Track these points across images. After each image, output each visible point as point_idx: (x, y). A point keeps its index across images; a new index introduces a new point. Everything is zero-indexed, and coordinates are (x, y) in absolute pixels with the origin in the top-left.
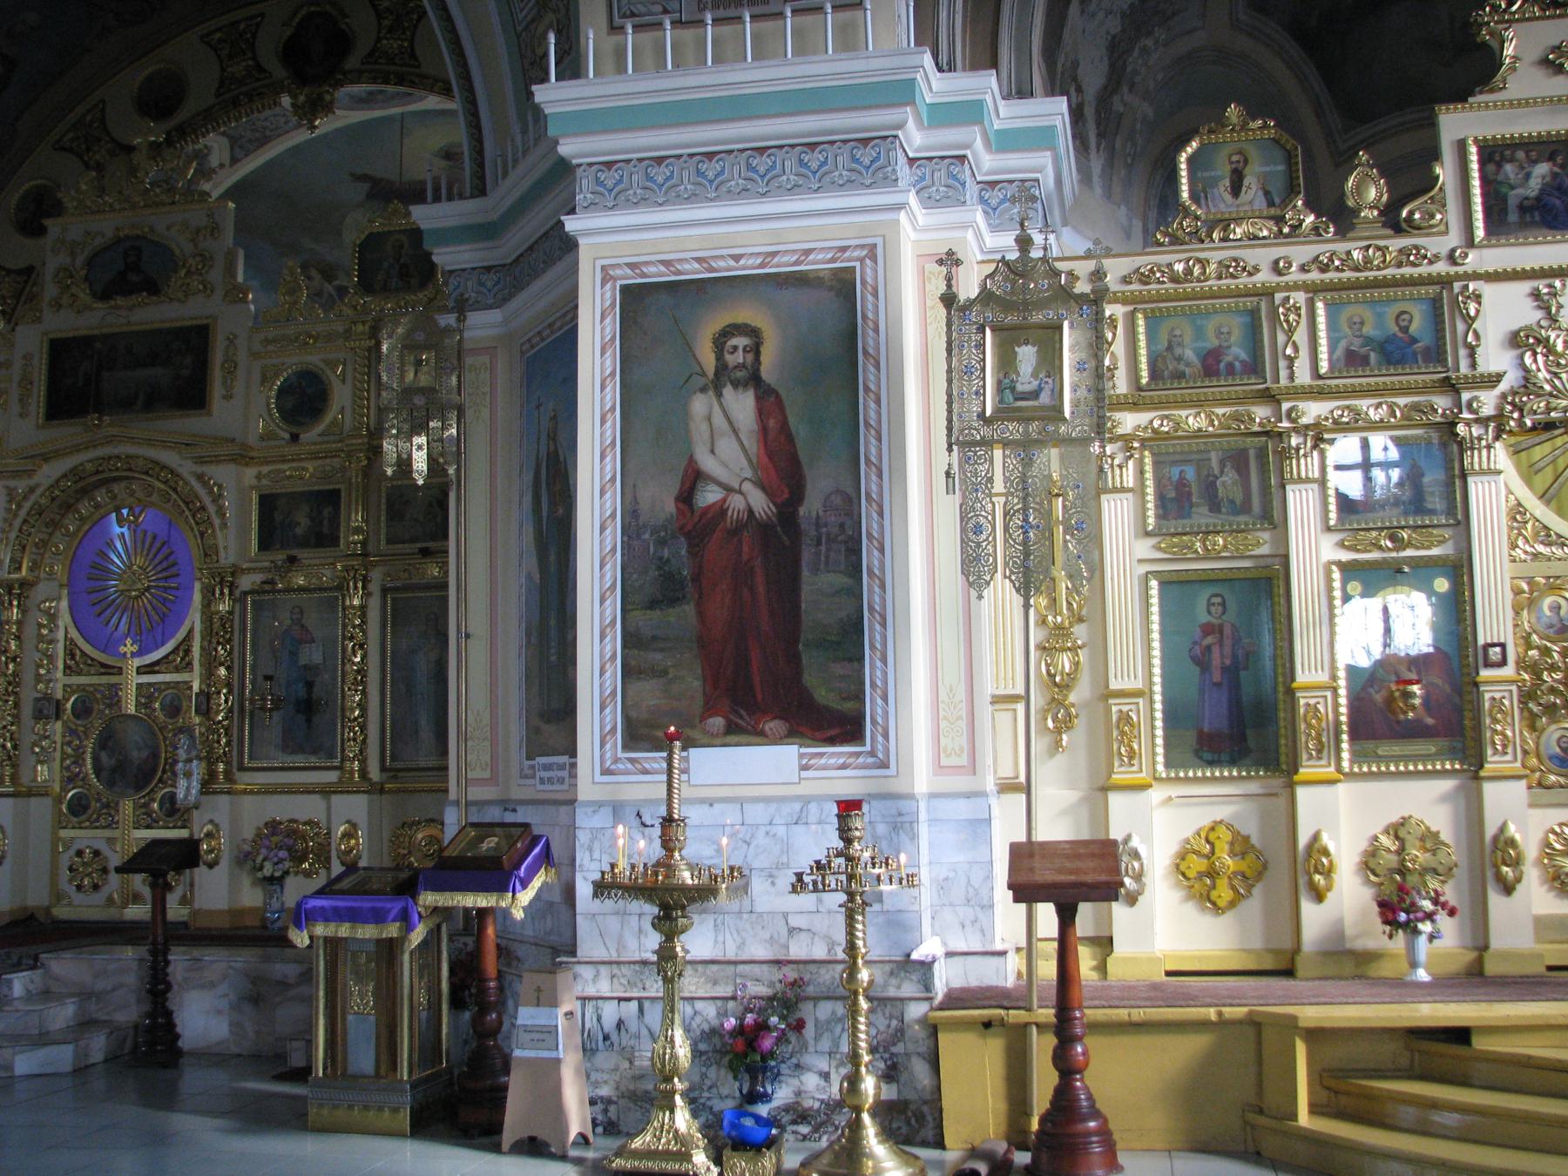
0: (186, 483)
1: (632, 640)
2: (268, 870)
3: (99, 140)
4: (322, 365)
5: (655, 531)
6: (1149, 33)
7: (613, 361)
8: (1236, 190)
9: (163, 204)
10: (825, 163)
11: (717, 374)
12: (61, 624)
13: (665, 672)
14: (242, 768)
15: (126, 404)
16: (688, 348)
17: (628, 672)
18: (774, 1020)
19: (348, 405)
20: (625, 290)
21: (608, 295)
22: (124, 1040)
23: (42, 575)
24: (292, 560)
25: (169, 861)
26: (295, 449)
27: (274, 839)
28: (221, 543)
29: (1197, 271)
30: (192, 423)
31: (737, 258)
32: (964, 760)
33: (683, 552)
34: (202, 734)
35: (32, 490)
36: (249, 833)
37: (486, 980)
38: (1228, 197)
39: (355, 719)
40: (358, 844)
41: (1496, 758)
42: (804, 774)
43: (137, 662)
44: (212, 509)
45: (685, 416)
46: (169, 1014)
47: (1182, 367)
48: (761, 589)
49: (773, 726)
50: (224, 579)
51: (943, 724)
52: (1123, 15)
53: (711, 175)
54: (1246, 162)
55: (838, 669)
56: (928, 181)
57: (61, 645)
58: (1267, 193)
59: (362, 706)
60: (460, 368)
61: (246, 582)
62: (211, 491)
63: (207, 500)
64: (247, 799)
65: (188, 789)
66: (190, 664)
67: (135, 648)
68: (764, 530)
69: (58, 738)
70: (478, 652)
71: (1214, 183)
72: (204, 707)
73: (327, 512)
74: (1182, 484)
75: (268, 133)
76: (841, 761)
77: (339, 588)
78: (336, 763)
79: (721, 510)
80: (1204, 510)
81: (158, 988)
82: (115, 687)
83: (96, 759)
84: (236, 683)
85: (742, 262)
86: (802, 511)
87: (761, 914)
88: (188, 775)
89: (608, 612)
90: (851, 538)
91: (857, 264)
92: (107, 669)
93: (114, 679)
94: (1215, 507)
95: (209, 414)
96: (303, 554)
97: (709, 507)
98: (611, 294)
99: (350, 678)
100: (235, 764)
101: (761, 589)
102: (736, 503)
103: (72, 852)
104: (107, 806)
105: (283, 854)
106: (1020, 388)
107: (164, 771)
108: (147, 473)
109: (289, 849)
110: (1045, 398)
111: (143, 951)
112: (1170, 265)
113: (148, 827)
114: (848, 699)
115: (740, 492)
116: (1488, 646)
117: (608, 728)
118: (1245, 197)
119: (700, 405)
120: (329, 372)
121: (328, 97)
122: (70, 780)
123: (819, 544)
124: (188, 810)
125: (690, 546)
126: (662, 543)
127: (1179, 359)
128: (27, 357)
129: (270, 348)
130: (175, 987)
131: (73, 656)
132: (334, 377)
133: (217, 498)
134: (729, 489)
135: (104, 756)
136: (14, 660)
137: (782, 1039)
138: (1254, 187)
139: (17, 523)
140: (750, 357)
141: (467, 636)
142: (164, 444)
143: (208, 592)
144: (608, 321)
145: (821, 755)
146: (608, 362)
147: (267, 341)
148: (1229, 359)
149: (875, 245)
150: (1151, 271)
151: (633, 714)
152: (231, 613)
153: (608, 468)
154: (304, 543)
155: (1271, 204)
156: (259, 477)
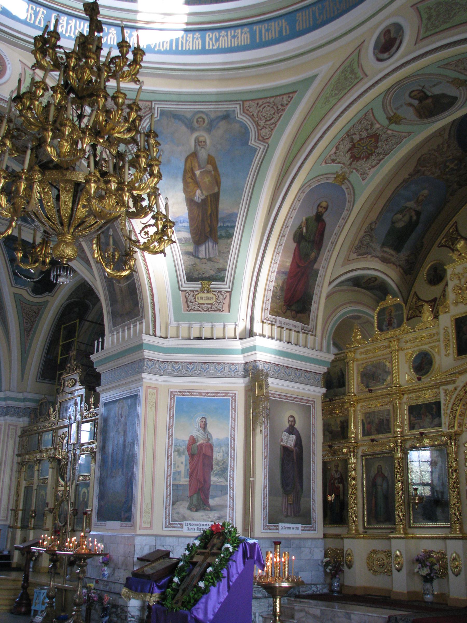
10: (193, 368)
14: (410, 527)
23: (464, 429)
35: (455, 389)
128: (445, 329)
136: (455, 471)
139: (450, 406)
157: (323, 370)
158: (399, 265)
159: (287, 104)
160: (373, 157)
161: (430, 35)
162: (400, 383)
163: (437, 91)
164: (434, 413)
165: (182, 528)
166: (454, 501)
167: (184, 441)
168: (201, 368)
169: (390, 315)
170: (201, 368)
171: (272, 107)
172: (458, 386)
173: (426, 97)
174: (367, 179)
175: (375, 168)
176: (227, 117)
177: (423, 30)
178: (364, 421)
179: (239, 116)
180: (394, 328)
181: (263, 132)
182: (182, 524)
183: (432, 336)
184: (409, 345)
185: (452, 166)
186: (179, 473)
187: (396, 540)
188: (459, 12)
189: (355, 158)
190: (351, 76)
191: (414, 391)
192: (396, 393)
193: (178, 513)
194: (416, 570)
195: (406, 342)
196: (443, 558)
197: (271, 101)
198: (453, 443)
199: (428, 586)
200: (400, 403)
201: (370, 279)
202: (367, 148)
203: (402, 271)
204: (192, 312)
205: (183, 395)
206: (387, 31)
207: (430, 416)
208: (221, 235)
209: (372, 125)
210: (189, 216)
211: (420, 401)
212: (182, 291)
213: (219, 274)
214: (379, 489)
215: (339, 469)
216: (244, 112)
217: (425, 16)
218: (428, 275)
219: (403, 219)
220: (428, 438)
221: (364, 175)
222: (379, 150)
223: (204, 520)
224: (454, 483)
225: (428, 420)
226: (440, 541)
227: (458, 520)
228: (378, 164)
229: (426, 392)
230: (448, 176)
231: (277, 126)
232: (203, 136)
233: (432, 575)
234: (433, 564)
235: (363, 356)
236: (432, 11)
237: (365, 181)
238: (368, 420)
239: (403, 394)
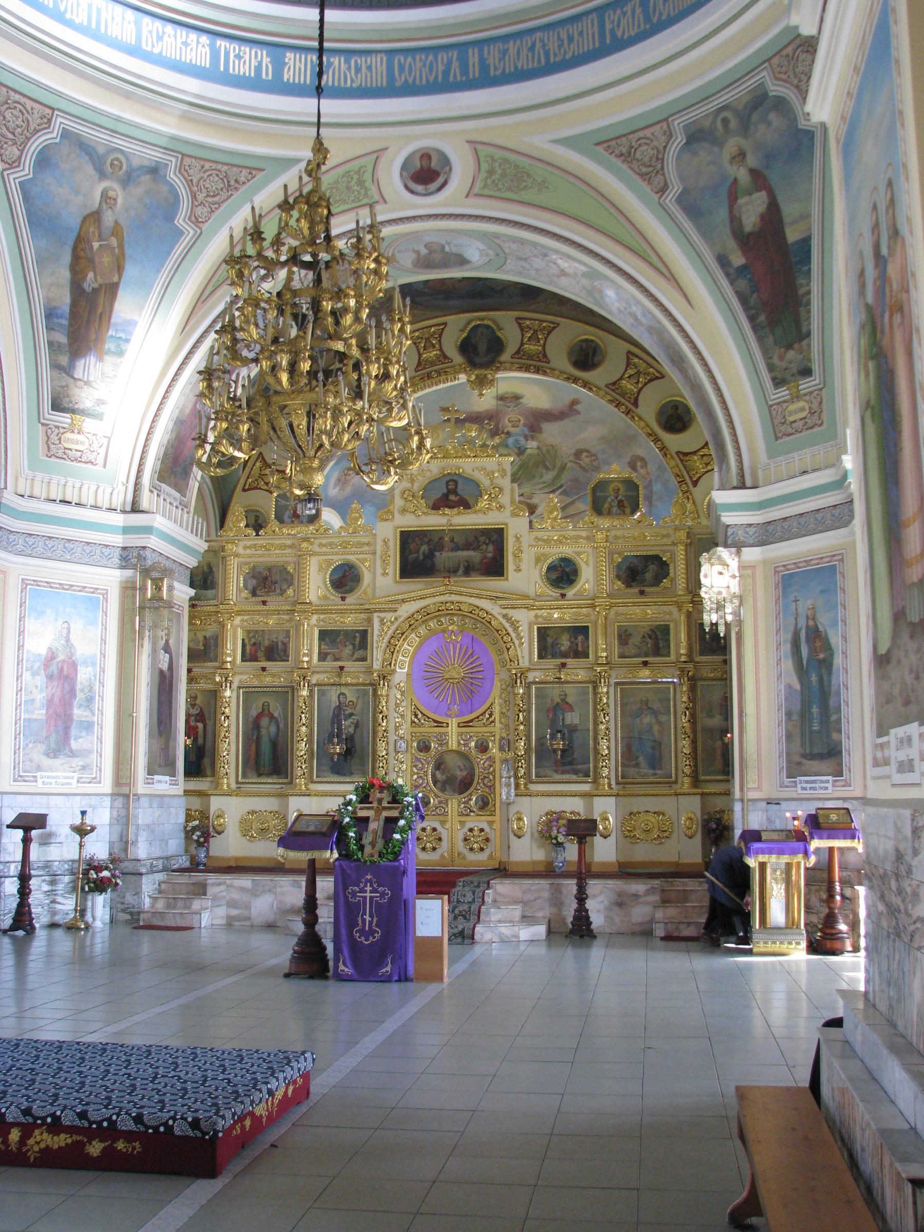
9: (469, 457)
14: (313, 782)
15: (452, 571)
19: (591, 578)
24: (564, 665)
30: (494, 584)
44: (513, 635)
63: (510, 630)
82: (446, 734)
83: (433, 776)
92: (439, 724)
95: (507, 579)
96: (570, 661)
103: (466, 830)
121: (489, 376)
131: (416, 716)
133: (516, 629)
154: (565, 655)
157: (192, 562)
159: (244, 183)
161: (491, 197)
164: (357, 643)
165: (36, 781)
167: (39, 655)
168: (65, 547)
170: (65, 547)
171: (222, 179)
172: (400, 617)
176: (155, 171)
177: (479, 184)
178: (246, 641)
179: (172, 176)
180: (302, 522)
181: (199, 211)
182: (795, 782)
186: (33, 701)
187: (217, 797)
188: (531, 188)
193: (31, 761)
197: (223, 170)
204: (53, 459)
205: (38, 586)
207: (351, 647)
208: (109, 349)
210: (71, 310)
212: (43, 424)
213: (97, 408)
214: (264, 732)
215: (198, 702)
216: (180, 172)
217: (485, 167)
223: (65, 771)
225: (348, 650)
231: (222, 208)
232: (114, 190)
235: (248, 551)
238: (253, 640)
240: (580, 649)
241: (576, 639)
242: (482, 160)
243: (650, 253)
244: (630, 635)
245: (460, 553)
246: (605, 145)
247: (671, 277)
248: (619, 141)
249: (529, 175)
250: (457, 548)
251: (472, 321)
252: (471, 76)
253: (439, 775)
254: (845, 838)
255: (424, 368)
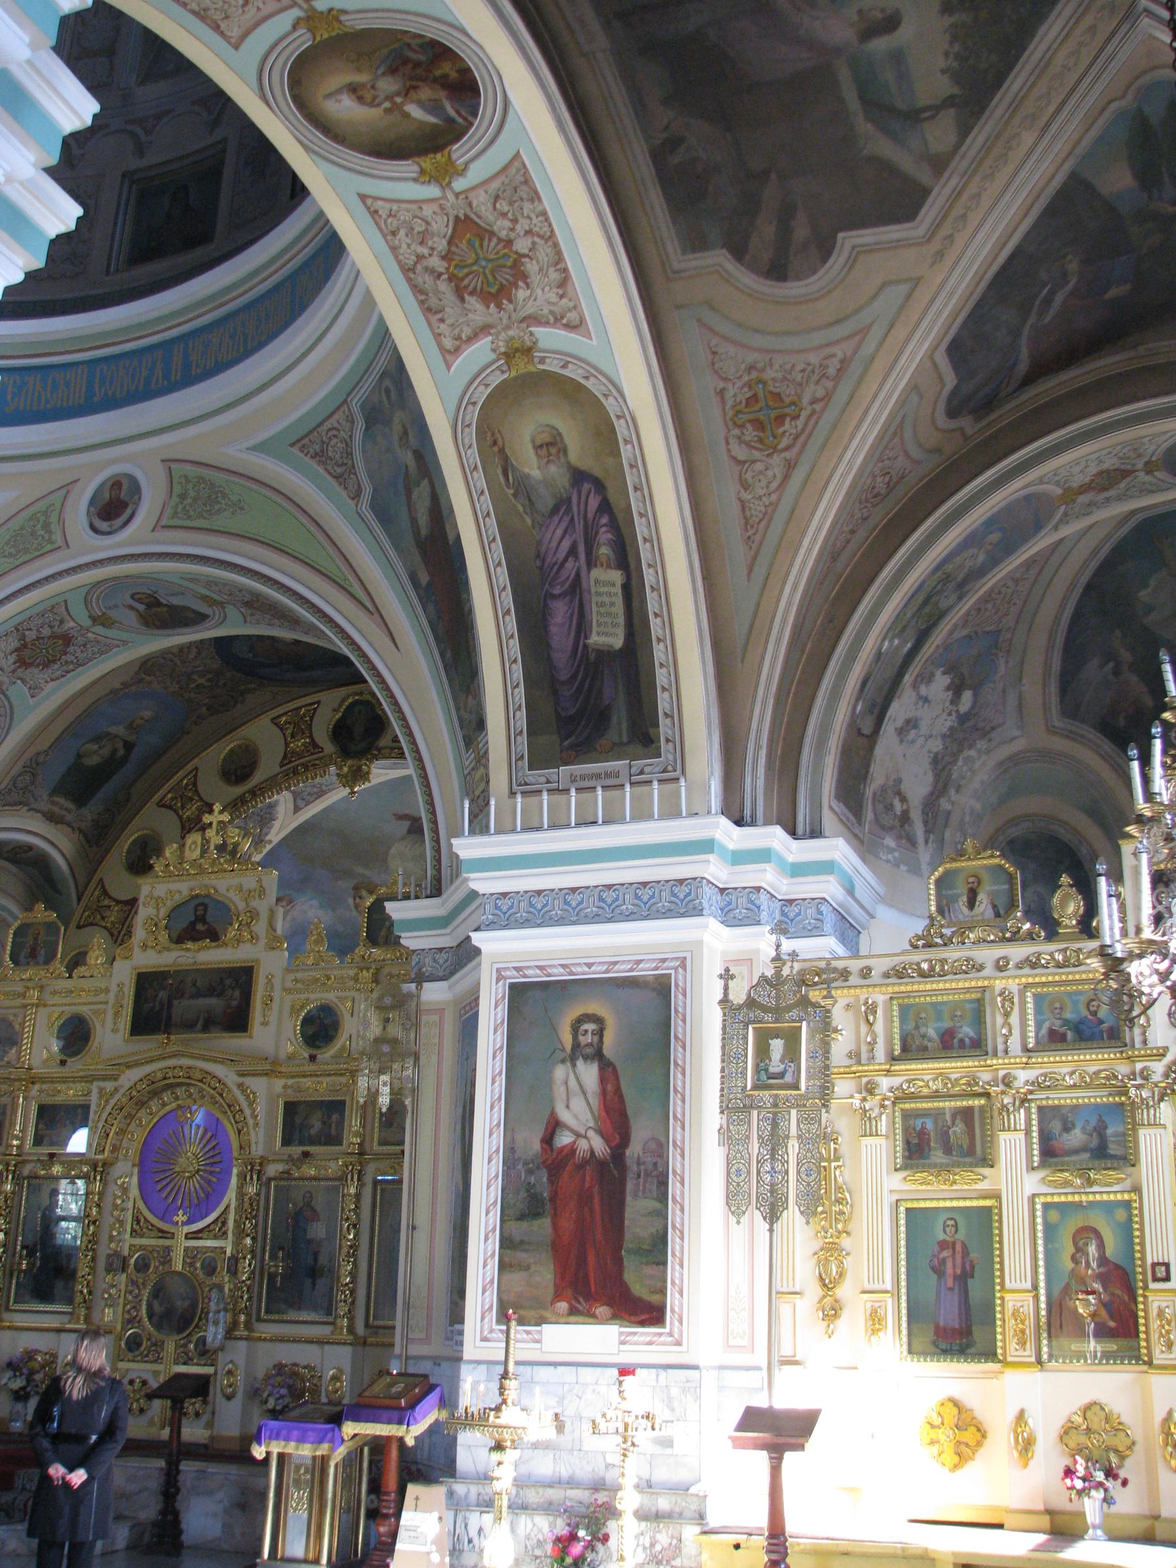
0: (230, 1091)
1: (507, 1243)
2: (271, 1404)
3: (191, 799)
4: (337, 1001)
5: (526, 1164)
6: (970, 747)
7: (501, 1038)
8: (971, 904)
11: (573, 1049)
12: (131, 1196)
13: (527, 1268)
14: (259, 1320)
16: (554, 1029)
17: (502, 1266)
18: (581, 1533)
20: (513, 986)
21: (500, 990)
22: (143, 1533)
25: (186, 1392)
26: (313, 1067)
27: (279, 1379)
28: (253, 1139)
29: (937, 969)
30: (234, 1042)
31: (589, 965)
32: (745, 1342)
33: (545, 1180)
34: (230, 1290)
35: (116, 1090)
36: (260, 1374)
37: (567, 1554)
38: (965, 910)
39: (347, 1284)
40: (342, 1386)
41: (1163, 1356)
42: (623, 1347)
43: (186, 1229)
44: (248, 1112)
45: (550, 1083)
46: (176, 1514)
47: (926, 1042)
48: (597, 1208)
49: (602, 1310)
50: (255, 1168)
51: (732, 1313)
52: (944, 736)
53: (574, 904)
54: (979, 883)
55: (649, 1270)
56: (733, 905)
57: (130, 1212)
58: (994, 907)
59: (353, 1275)
60: (417, 1025)
61: (272, 1170)
62: (248, 1096)
64: (262, 1345)
65: (215, 1334)
66: (225, 1233)
67: (185, 1218)
68: (601, 1166)
69: (123, 1287)
70: (422, 1237)
71: (955, 899)
72: (233, 1268)
73: (335, 1117)
74: (922, 1133)
75: (324, 788)
76: (648, 1339)
77: (339, 1179)
78: (331, 1319)
79: (572, 1149)
80: (940, 1153)
81: (170, 1490)
82: (168, 1249)
84: (259, 1251)
85: (593, 968)
86: (628, 1152)
87: (587, 1452)
88: (216, 1323)
89: (491, 1221)
90: (662, 1173)
91: (672, 972)
92: (163, 1234)
93: (167, 1242)
94: (948, 1150)
97: (566, 1146)
98: (502, 990)
99: (345, 1250)
100: (254, 1317)
101: (597, 1208)
102: (583, 1145)
104: (155, 1344)
105: (283, 1391)
106: (771, 1070)
107: (200, 1319)
108: (201, 1081)
109: (290, 1387)
110: (788, 1078)
111: (162, 1463)
112: (918, 964)
113: (185, 1364)
114: (655, 1292)
115: (585, 1137)
116: (1154, 1265)
117: (487, 1307)
118: (978, 909)
119: (560, 1072)
120: (342, 1007)
122: (130, 1322)
123: (639, 1176)
124: (215, 1352)
125: (550, 1175)
126: (530, 1172)
127: (923, 1036)
128: (120, 986)
129: (299, 985)
130: (183, 1491)
131: (138, 1223)
132: (344, 1009)
134: (578, 1135)
135: (156, 1304)
136: (94, 1222)
137: (590, 1546)
138: (985, 902)
140: (596, 1038)
141: (414, 1228)
142: (214, 1060)
143: (242, 1177)
144: (500, 1008)
145: (635, 1334)
146: (499, 1039)
147: (296, 981)
148: (960, 1036)
149: (685, 958)
150: (904, 968)
151: (505, 1297)
152: (258, 1194)
153: (496, 1116)
155: (997, 915)
156: (285, 1087)
158: (79, 829)
160: (56, 667)
162: (32, 1062)
163: (176, 601)
166: (83, 1270)
169: (36, 939)
172: (122, 1086)
173: (159, 604)
174: (40, 697)
175: (58, 682)
177: (169, 512)
183: (98, 991)
184: (57, 999)
185: (201, 681)
189: (23, 663)
190: (42, 532)
191: (52, 1080)
192: (20, 1080)
194: (4, 1381)
195: (54, 993)
196: (52, 1362)
198: (98, 1178)
199: (19, 1406)
200: (25, 1098)
201: (20, 847)
202: (47, 652)
203: (82, 838)
206: (116, 484)
209: (62, 622)
211: (59, 1099)
217: (177, 490)
218: (129, 852)
219: (101, 752)
220: (62, 1163)
221: (34, 690)
222: (69, 658)
224: (90, 1242)
226: (52, 1335)
227: (85, 1301)
228: (63, 676)
229: (72, 1085)
230: (193, 695)
233: (28, 1389)
234: (32, 1372)
236: (190, 486)
237: (35, 699)
239: (33, 1083)
240: (333, 1132)
241: (329, 1117)
242: (175, 480)
243: (351, 578)
244: (397, 1112)
245: (202, 1002)
246: (300, 444)
247: (374, 611)
248: (311, 437)
249: (224, 495)
250: (199, 994)
251: (349, 696)
252: (173, 379)
253: (157, 1308)
254: (389, 1422)
255: (291, 762)
